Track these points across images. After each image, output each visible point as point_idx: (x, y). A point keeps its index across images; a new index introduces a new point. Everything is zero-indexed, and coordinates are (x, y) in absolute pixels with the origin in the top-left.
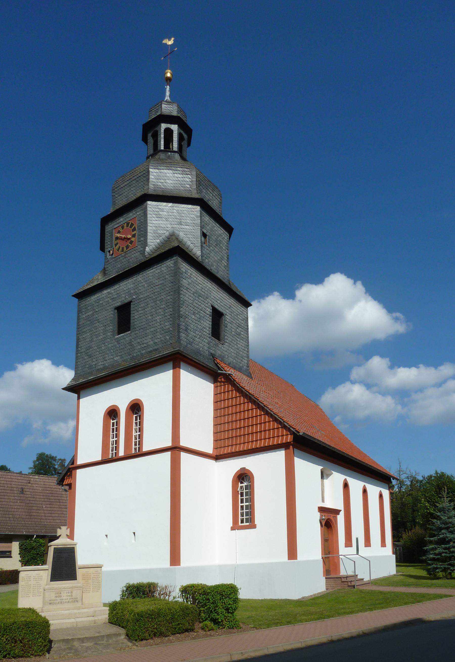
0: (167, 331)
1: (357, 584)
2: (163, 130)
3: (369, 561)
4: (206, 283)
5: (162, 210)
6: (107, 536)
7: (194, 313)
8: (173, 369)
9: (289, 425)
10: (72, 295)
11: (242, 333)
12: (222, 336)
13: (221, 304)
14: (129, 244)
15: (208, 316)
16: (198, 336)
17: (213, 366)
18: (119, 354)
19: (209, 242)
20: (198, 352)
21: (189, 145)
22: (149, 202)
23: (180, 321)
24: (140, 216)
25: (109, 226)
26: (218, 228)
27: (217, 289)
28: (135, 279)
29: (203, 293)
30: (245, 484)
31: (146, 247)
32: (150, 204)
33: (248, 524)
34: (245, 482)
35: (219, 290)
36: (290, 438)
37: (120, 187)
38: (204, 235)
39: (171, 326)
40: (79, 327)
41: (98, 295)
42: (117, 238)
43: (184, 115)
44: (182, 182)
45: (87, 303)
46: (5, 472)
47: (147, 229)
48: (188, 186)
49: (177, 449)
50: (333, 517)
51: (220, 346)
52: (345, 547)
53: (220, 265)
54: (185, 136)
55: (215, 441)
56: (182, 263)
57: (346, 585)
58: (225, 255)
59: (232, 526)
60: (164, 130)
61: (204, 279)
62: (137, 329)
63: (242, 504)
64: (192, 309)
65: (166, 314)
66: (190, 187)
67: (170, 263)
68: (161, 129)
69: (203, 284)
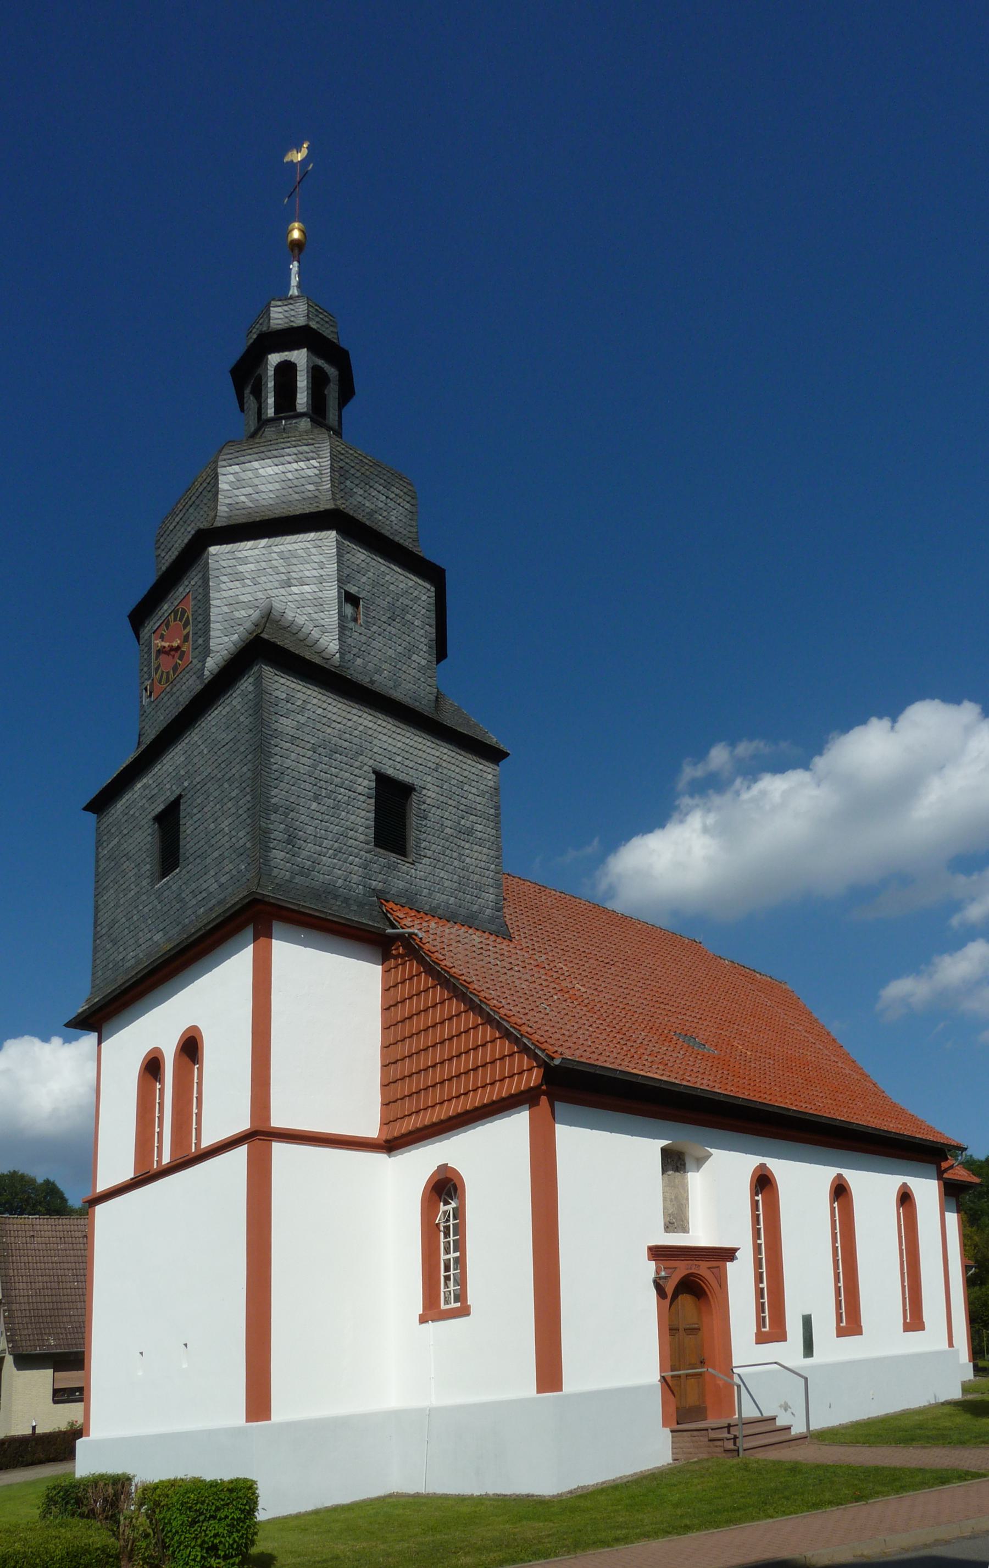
0: (241, 850)
1: (746, 1446)
2: (273, 369)
3: (803, 1380)
4: (355, 718)
5: (244, 561)
6: (186, 1345)
7: (316, 798)
8: (254, 941)
9: (533, 1043)
10: (82, 807)
11: (480, 827)
12: (411, 843)
13: (407, 762)
14: (178, 661)
15: (362, 798)
16: (331, 852)
17: (374, 921)
18: (161, 927)
19: (366, 615)
20: (329, 892)
21: (347, 393)
22: (213, 549)
23: (269, 822)
24: (195, 588)
25: (146, 630)
26: (396, 576)
27: (394, 729)
28: (186, 741)
29: (346, 744)
30: (453, 1205)
31: (206, 659)
32: (214, 553)
33: (458, 1305)
34: (452, 1200)
35: (399, 731)
36: (534, 1078)
37: (167, 533)
38: (351, 599)
39: (248, 837)
40: (98, 877)
41: (127, 797)
42: (161, 651)
43: (327, 322)
44: (296, 483)
45: (111, 820)
46: (28, 1218)
47: (209, 615)
48: (311, 487)
49: (258, 1137)
50: (709, 1268)
51: (404, 867)
52: (756, 1343)
53: (405, 668)
54: (332, 371)
55: (386, 1105)
56: (276, 678)
57: (718, 1450)
58: (423, 639)
59: (421, 1312)
60: (275, 370)
61: (349, 709)
62: (191, 859)
63: (448, 1257)
64: (308, 787)
65: (240, 812)
66: (317, 490)
67: (246, 685)
68: (267, 369)
69: (345, 721)
